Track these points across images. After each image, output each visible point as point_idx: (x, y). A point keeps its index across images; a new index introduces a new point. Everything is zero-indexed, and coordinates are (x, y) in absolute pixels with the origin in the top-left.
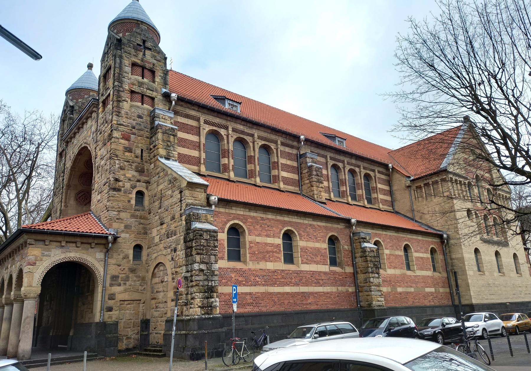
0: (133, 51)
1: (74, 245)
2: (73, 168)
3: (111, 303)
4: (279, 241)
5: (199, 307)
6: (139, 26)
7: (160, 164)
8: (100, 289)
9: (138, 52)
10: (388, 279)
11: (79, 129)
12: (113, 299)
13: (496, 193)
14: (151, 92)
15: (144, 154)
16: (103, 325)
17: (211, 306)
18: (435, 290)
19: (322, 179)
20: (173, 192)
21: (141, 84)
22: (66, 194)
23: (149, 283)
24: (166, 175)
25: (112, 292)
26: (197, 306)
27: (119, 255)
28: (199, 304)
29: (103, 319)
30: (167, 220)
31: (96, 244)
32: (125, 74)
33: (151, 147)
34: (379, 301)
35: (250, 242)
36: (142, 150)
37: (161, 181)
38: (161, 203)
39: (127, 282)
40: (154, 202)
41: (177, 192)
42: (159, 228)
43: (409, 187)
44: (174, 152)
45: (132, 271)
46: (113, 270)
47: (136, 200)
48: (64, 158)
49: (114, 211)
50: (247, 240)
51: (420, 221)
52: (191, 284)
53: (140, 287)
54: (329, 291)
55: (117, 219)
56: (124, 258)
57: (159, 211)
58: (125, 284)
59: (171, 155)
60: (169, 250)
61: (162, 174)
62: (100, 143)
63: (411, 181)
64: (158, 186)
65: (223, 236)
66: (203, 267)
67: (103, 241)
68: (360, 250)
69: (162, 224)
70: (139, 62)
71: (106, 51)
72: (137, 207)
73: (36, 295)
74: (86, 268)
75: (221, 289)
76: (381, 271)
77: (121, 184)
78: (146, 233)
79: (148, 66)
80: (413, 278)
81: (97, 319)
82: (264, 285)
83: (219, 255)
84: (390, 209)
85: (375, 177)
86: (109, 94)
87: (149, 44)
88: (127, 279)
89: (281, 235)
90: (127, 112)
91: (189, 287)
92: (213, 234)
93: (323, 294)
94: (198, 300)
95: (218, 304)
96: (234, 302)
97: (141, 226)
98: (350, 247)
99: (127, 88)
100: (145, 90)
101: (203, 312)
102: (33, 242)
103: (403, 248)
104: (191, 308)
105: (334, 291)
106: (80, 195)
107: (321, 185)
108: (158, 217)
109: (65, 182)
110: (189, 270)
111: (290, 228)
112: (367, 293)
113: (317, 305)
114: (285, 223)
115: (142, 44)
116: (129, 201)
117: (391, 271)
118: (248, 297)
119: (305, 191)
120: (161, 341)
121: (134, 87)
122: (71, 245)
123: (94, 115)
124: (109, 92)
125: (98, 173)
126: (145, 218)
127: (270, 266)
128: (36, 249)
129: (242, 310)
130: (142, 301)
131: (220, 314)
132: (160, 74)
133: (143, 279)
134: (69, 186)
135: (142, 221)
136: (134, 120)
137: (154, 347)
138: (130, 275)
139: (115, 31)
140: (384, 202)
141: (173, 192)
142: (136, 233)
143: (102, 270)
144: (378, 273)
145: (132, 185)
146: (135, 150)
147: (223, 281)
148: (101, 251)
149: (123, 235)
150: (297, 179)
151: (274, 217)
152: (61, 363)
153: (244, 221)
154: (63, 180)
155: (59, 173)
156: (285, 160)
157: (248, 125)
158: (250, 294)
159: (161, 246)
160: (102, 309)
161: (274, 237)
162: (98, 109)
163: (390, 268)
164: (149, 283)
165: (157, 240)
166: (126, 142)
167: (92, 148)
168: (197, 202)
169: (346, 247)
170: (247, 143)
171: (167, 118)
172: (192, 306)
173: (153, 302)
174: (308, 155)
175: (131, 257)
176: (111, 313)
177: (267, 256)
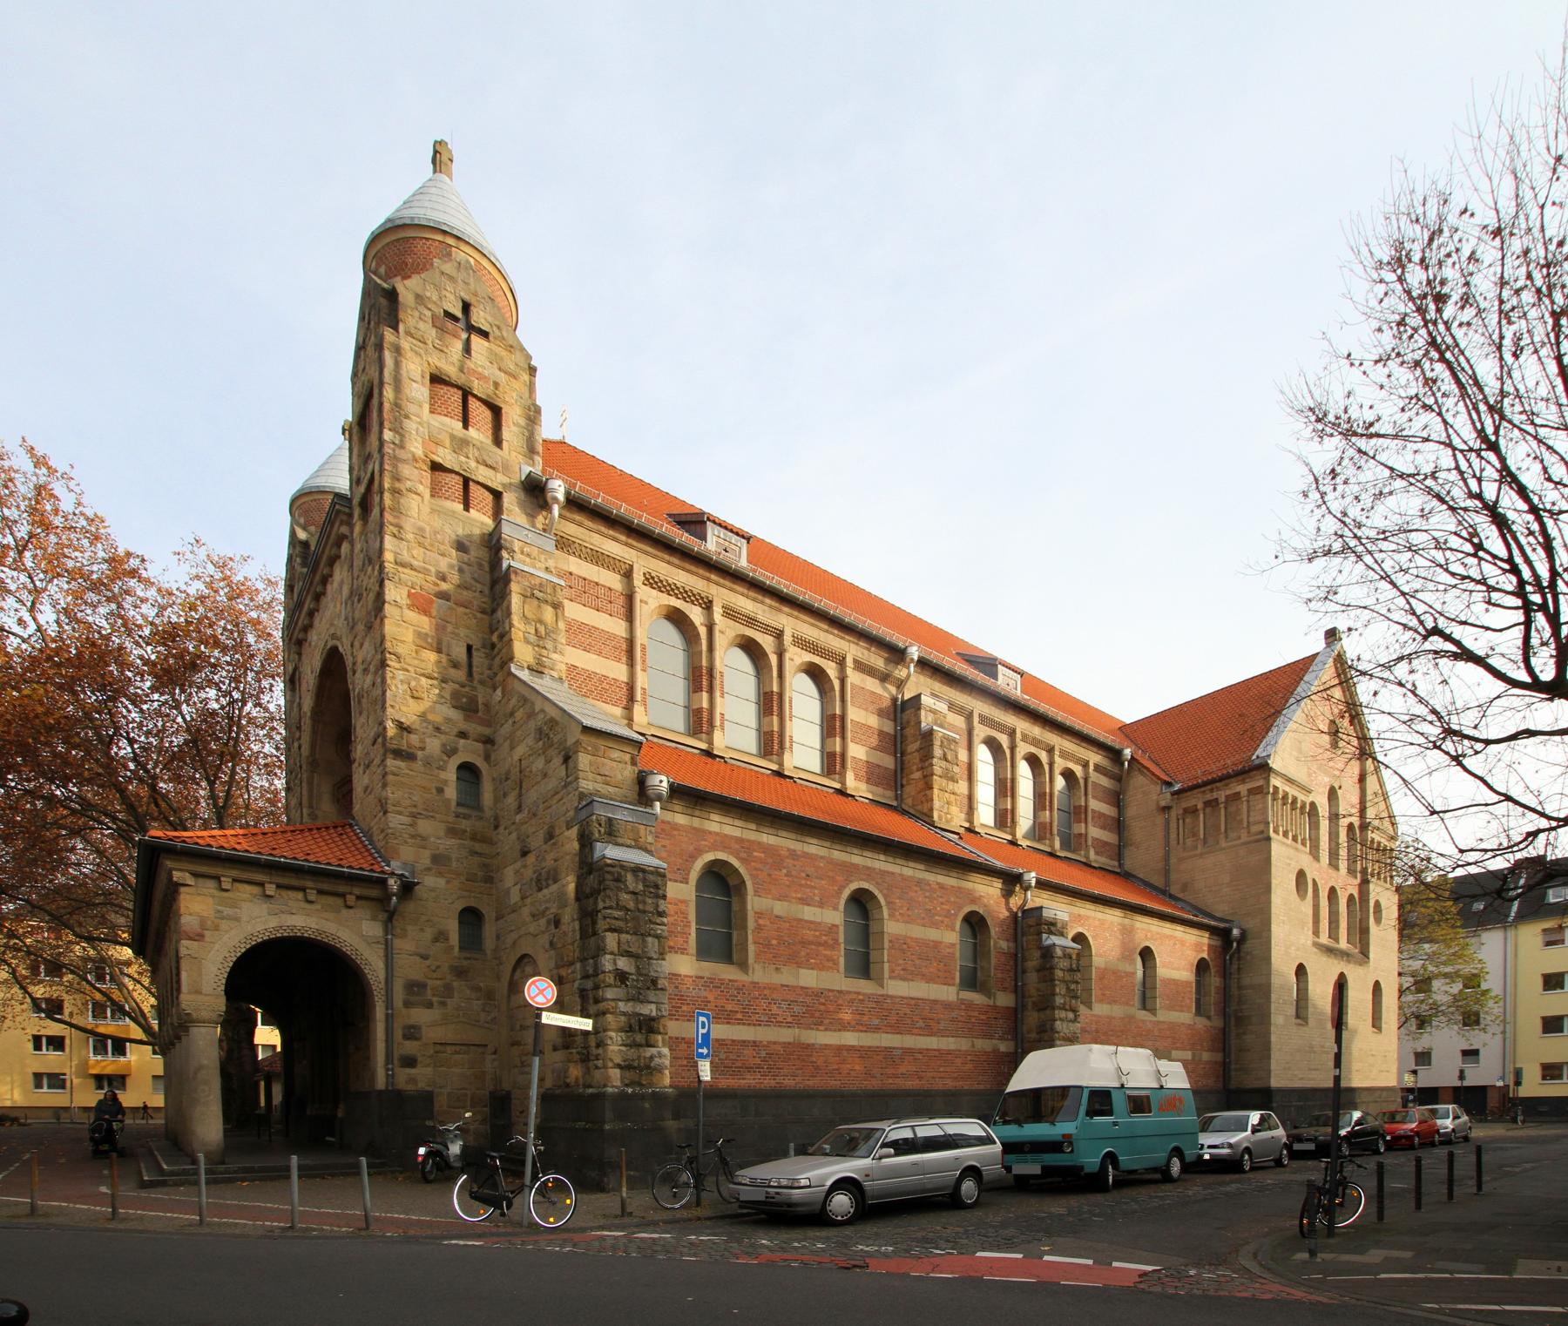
0: (431, 333)
1: (300, 895)
3: (410, 1047)
4: (835, 916)
5: (619, 1066)
6: (450, 254)
7: (517, 685)
8: (380, 1012)
9: (449, 339)
10: (1094, 1027)
11: (318, 597)
13: (1063, 981)
14: (490, 473)
15: (475, 661)
16: (395, 1098)
17: (648, 1067)
19: (956, 769)
20: (548, 762)
22: (310, 783)
24: (531, 715)
25: (411, 1022)
30: (536, 842)
31: (359, 898)
33: (495, 638)
35: (759, 915)
36: (469, 648)
37: (519, 733)
38: (520, 795)
40: (505, 795)
41: (557, 761)
42: (519, 864)
43: (1167, 809)
44: (554, 656)
45: (460, 973)
46: (410, 967)
49: (400, 813)
51: (1180, 895)
53: (483, 1015)
54: (952, 1047)
55: (413, 837)
57: (518, 817)
58: (443, 1004)
60: (543, 921)
61: (519, 714)
62: (360, 627)
63: (1173, 794)
64: (512, 748)
65: (682, 893)
66: (623, 964)
67: (374, 892)
68: (1037, 954)
69: (524, 854)
72: (461, 810)
73: (214, 1016)
75: (674, 1028)
76: (1082, 1009)
77: (414, 739)
78: (489, 880)
79: (478, 388)
80: (1149, 1026)
81: (381, 1082)
82: (789, 1025)
84: (1112, 864)
85: (1086, 780)
87: (480, 317)
88: (448, 991)
89: (842, 902)
90: (422, 529)
92: (653, 883)
95: (667, 1063)
96: (701, 1056)
97: (477, 859)
98: (1012, 945)
99: (419, 453)
100: (473, 464)
102: (190, 880)
107: (951, 786)
108: (514, 835)
109: (305, 751)
111: (865, 885)
113: (920, 1078)
114: (851, 870)
115: (459, 314)
116: (440, 791)
117: (1100, 1009)
118: (748, 1052)
119: (909, 801)
121: (441, 450)
122: (291, 894)
123: (345, 547)
126: (490, 842)
127: (809, 978)
128: (199, 898)
129: (726, 1083)
130: (490, 1049)
133: (489, 995)
134: (314, 764)
135: (478, 847)
136: (443, 555)
138: (455, 984)
139: (382, 270)
140: (1101, 846)
141: (548, 762)
143: (381, 965)
144: (1074, 1011)
145: (444, 745)
146: (449, 646)
147: (685, 1008)
148: (374, 918)
149: (430, 881)
150: (892, 731)
151: (823, 852)
152: (272, 1179)
153: (744, 855)
156: (863, 713)
157: (768, 601)
158: (755, 1044)
159: (526, 911)
161: (821, 905)
162: (351, 526)
163: (1101, 1001)
165: (515, 896)
168: (611, 789)
169: (1004, 945)
170: (765, 654)
171: (535, 552)
173: (515, 1051)
175: (454, 938)
176: (412, 1071)
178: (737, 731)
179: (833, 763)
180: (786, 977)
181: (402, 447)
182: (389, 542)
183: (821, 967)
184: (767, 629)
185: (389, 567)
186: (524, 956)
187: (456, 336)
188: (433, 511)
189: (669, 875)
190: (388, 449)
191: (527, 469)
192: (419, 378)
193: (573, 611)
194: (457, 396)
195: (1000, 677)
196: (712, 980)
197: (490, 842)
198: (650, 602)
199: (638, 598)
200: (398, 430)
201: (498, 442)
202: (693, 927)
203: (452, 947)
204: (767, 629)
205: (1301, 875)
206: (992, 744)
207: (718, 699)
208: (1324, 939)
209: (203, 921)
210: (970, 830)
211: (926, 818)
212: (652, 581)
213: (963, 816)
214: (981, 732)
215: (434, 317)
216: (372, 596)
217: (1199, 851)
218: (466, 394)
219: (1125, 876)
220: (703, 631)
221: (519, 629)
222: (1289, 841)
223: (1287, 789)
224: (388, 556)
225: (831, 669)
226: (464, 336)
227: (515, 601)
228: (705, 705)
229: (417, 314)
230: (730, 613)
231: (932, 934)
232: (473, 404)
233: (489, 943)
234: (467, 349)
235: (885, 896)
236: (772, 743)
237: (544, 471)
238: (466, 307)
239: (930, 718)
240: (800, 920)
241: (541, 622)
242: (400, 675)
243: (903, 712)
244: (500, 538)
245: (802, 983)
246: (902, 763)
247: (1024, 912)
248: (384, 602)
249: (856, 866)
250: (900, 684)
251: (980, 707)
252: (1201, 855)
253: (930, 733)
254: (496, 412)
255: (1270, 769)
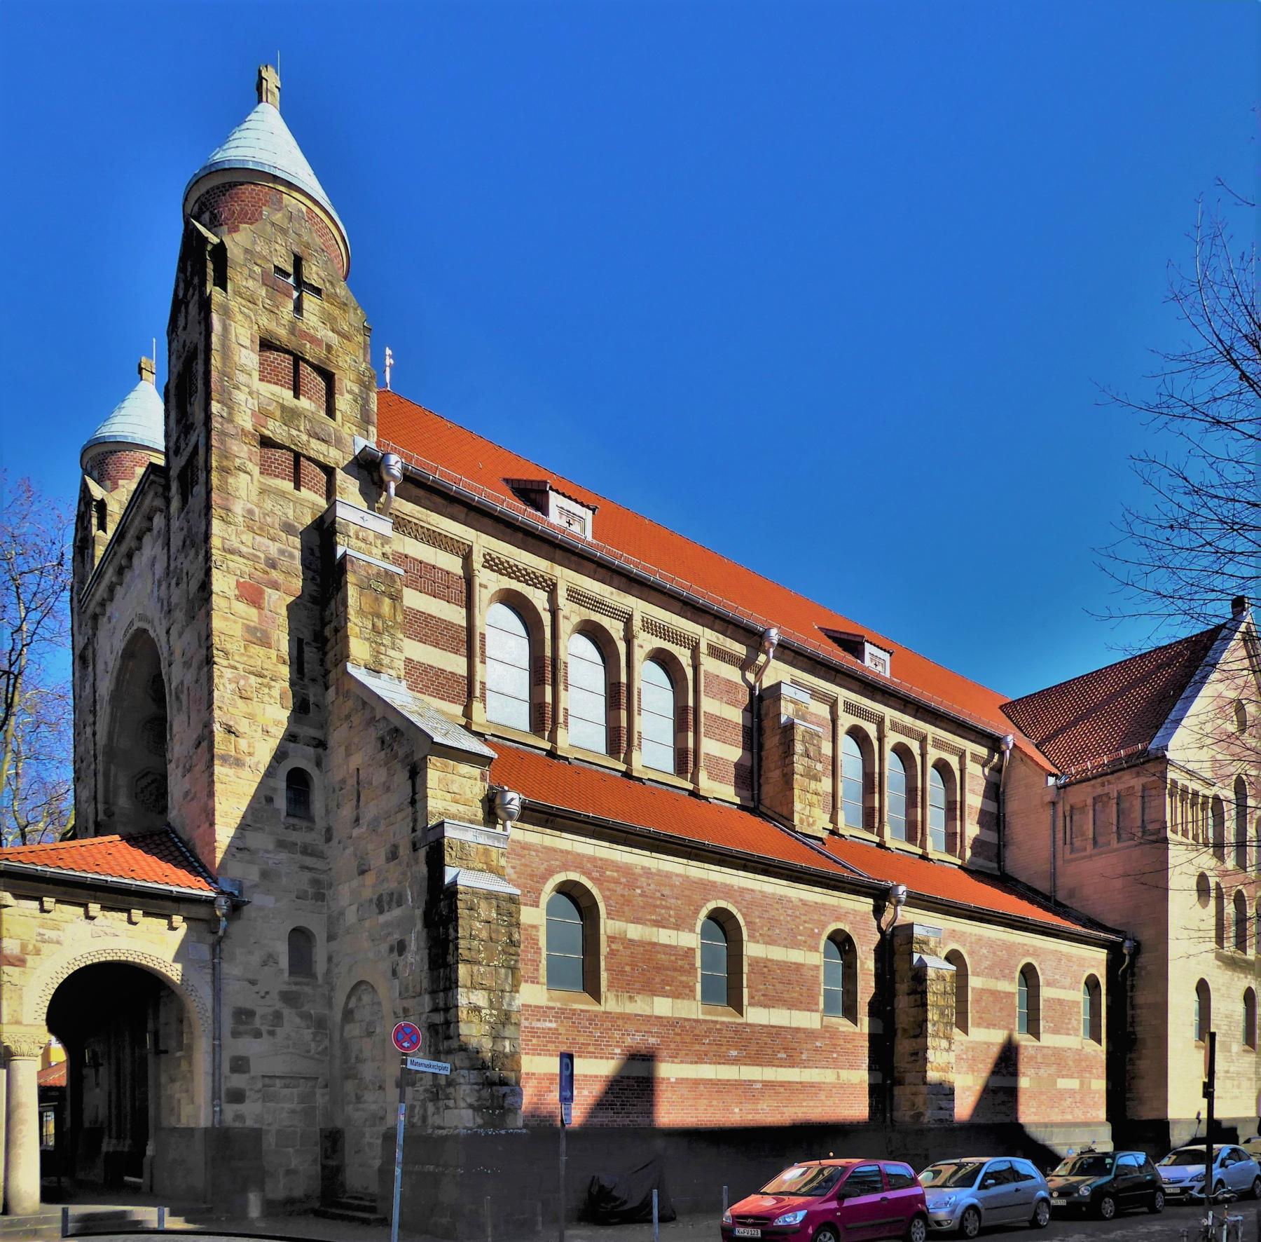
2: (116, 697)
3: (238, 1081)
9: (280, 298)
11: (120, 571)
12: (244, 1072)
14: (322, 447)
17: (502, 1107)
18: (1082, 1084)
19: (819, 767)
21: (290, 416)
23: (337, 1036)
26: (462, 1104)
27: (250, 953)
28: (469, 1100)
29: (220, 1122)
32: (242, 378)
34: (941, 1109)
35: (612, 939)
39: (278, 1030)
42: (355, 883)
44: (391, 652)
45: (289, 998)
47: (289, 801)
48: (90, 668)
50: (602, 931)
52: (446, 1043)
56: (265, 964)
57: (356, 832)
59: (386, 661)
62: (179, 615)
64: (348, 754)
69: (362, 872)
70: (282, 333)
71: (181, 294)
74: (169, 988)
78: (320, 897)
79: (310, 351)
83: (523, 969)
86: (196, 447)
90: (250, 512)
91: (439, 1052)
92: (508, 906)
93: (799, 1086)
94: (467, 1088)
97: (307, 875)
99: (249, 426)
100: (305, 437)
101: (480, 1121)
103: (1017, 974)
104: (447, 1107)
105: (827, 1080)
106: (143, 783)
107: (814, 785)
109: (102, 739)
110: (441, 1005)
112: (914, 1089)
114: (708, 888)
120: (374, 1188)
121: (271, 424)
124: (193, 439)
125: (179, 710)
126: (320, 855)
131: (525, 1126)
132: (349, 384)
135: (309, 861)
136: (273, 539)
137: (356, 1198)
142: (293, 896)
153: (596, 875)
154: (94, 734)
155: (85, 709)
160: (215, 1095)
161: (677, 927)
163: (978, 1025)
164: (337, 1036)
166: (253, 612)
167: (157, 632)
168: (462, 808)
171: (371, 538)
172: (451, 1103)
174: (785, 690)
175: (284, 962)
177: (657, 980)
178: (583, 732)
179: (685, 760)
180: (640, 1006)
181: (230, 421)
182: (216, 526)
183: (676, 995)
184: (614, 613)
185: (216, 554)
186: (360, 983)
187: (290, 296)
188: (263, 491)
189: (522, 900)
190: (216, 424)
191: (361, 443)
192: (247, 343)
193: (414, 599)
194: (287, 361)
195: (867, 657)
196: (563, 1011)
197: (320, 855)
198: (489, 582)
199: (477, 581)
200: (228, 403)
201: (331, 411)
202: (544, 953)
203: (281, 971)
204: (614, 613)
205: (1202, 878)
206: (857, 734)
207: (562, 694)
208: (1229, 946)
209: (24, 947)
210: (833, 832)
211: (784, 819)
212: (492, 563)
213: (828, 817)
214: (846, 721)
215: (264, 272)
216: (194, 585)
217: (1088, 852)
218: (298, 359)
219: (1004, 881)
220: (546, 618)
221: (356, 626)
222: (1191, 841)
223: (1187, 783)
224: (216, 542)
225: (683, 655)
226: (295, 294)
227: (352, 592)
228: (548, 698)
229: (246, 272)
230: (576, 596)
231: (796, 956)
232: (305, 370)
233: (320, 966)
234: (298, 308)
235: (744, 916)
236: (619, 739)
237: (378, 443)
238: (298, 261)
239: (791, 707)
240: (654, 944)
241: (379, 616)
242: (228, 673)
243: (761, 705)
244: (334, 522)
245: (657, 1013)
246: (760, 759)
247: (894, 928)
248: (211, 593)
249: (713, 885)
250: (759, 672)
251: (844, 695)
252: (1091, 856)
253: (790, 727)
254: (329, 378)
255: (1167, 761)
